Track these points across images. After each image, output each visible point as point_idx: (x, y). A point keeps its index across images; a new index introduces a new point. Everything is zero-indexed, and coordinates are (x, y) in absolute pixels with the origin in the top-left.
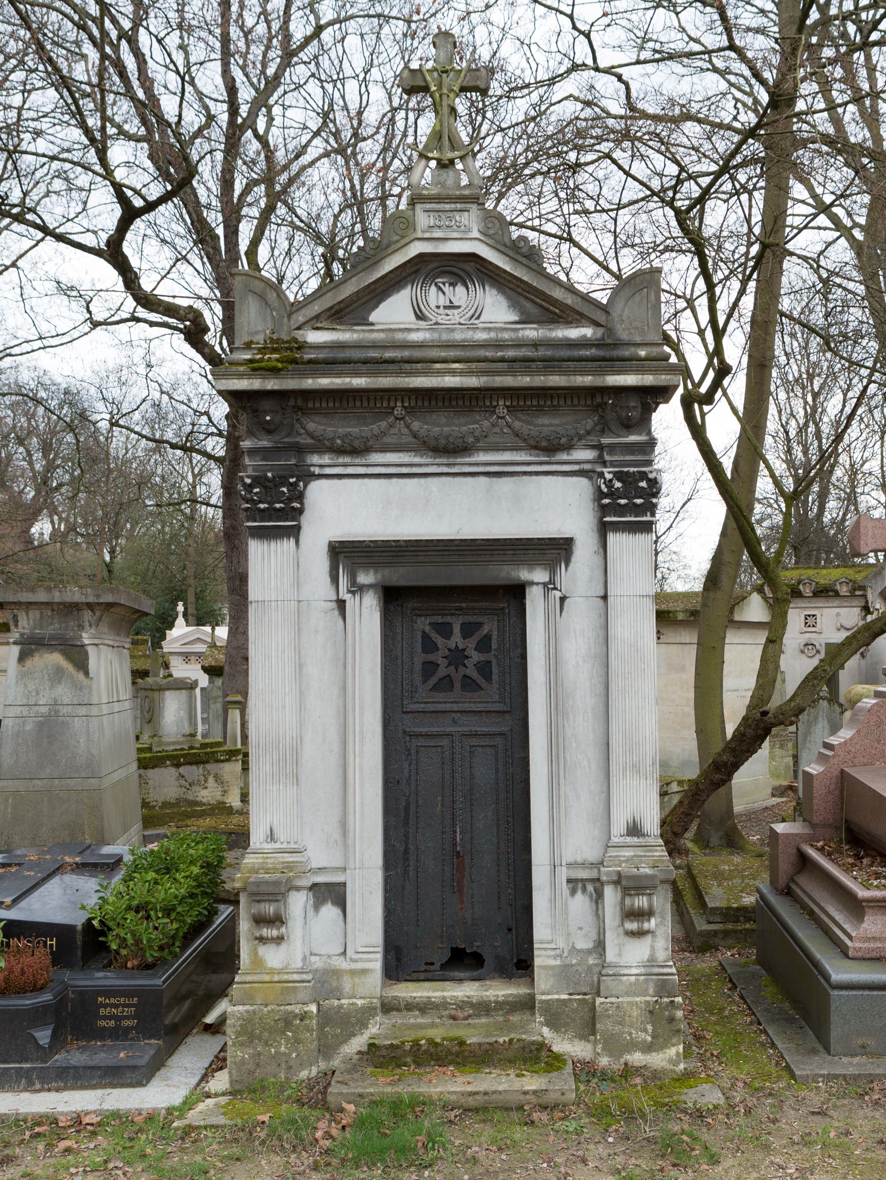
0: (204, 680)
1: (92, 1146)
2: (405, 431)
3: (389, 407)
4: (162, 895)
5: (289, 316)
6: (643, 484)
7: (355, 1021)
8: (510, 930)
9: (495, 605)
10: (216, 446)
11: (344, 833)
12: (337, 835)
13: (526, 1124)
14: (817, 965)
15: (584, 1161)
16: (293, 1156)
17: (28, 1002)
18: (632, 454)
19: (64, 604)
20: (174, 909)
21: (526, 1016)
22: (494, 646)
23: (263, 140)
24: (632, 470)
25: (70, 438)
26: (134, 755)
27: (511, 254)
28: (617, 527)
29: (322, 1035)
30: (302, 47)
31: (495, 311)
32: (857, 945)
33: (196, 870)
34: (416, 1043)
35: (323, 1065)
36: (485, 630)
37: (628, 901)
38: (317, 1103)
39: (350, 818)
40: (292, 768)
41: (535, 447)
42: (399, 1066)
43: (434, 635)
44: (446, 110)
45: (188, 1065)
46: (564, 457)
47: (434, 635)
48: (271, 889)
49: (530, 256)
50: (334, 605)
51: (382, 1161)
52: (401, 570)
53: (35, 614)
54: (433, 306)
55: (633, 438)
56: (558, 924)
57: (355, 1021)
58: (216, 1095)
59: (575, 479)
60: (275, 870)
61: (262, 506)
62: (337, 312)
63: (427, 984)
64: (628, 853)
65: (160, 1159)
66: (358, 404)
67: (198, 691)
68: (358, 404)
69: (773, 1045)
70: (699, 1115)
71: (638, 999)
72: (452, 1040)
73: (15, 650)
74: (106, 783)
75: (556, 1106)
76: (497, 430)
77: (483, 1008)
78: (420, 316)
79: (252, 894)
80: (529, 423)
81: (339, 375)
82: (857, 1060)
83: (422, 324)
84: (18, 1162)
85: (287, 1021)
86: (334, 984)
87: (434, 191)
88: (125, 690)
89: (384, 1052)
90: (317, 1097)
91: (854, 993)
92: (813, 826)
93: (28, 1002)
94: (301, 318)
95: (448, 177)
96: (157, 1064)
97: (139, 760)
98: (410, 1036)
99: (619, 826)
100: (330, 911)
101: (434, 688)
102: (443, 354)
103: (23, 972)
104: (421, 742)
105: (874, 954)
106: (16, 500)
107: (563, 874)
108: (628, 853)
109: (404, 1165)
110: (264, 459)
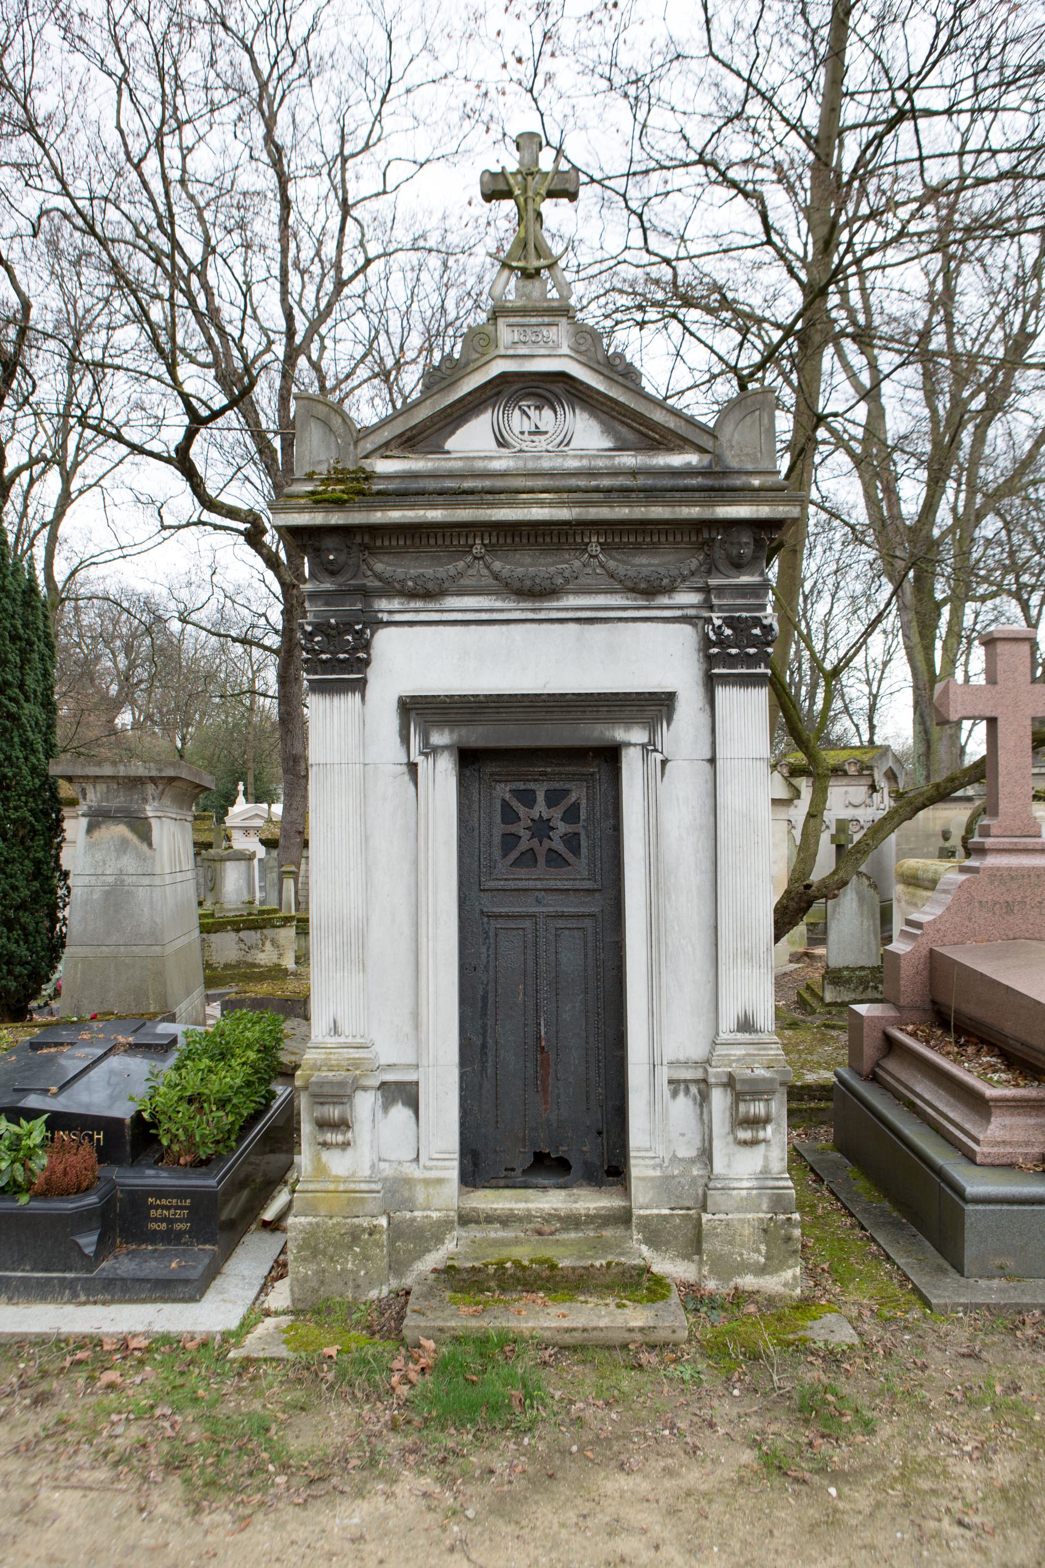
0: (261, 851)
1: (138, 1380)
2: (485, 572)
3: (466, 545)
4: (216, 1088)
5: (356, 443)
6: (757, 631)
7: (427, 1236)
8: (600, 1133)
9: (584, 770)
10: (273, 641)
11: (417, 1027)
12: (408, 1028)
13: (633, 1368)
14: (939, 1172)
15: (712, 1425)
16: (367, 1407)
17: (69, 1205)
18: (744, 597)
19: (128, 777)
20: (229, 1100)
21: (619, 1232)
22: (583, 815)
23: (316, 366)
24: (744, 614)
25: (148, 641)
26: (195, 922)
27: (606, 372)
28: (727, 680)
29: (393, 1250)
30: (352, 278)
31: (585, 437)
32: (986, 1150)
33: (252, 1055)
34: (500, 1265)
35: (394, 1283)
36: (573, 798)
37: (742, 1107)
38: (389, 1331)
39: (423, 1010)
40: (357, 952)
41: (633, 590)
42: (482, 1291)
43: (515, 804)
44: (531, 215)
45: (246, 1273)
46: (665, 600)
47: (515, 804)
48: (335, 1091)
49: (626, 374)
50: (404, 769)
51: (472, 1421)
52: (480, 729)
53: (101, 787)
54: (516, 431)
55: (745, 579)
56: (658, 1130)
57: (427, 1236)
58: (277, 1314)
59: (677, 626)
60: (338, 1067)
61: (324, 656)
62: (409, 439)
63: (507, 1192)
64: (740, 1051)
65: (212, 1406)
66: (432, 541)
67: (256, 862)
68: (432, 541)
69: (888, 1258)
70: (833, 1358)
71: (750, 1216)
72: (541, 1262)
73: (84, 822)
74: (169, 949)
75: (666, 1344)
76: (589, 570)
77: (572, 1221)
78: (502, 443)
79: (314, 1095)
80: (625, 563)
81: (412, 507)
82: (995, 1283)
83: (504, 451)
84: (55, 1401)
85: (354, 1236)
86: (406, 1194)
87: (519, 303)
88: (187, 861)
89: (465, 1276)
90: (389, 1321)
91: (991, 1207)
92: (898, 1007)
93: (69, 1205)
94: (368, 445)
95: (534, 288)
96: (213, 1272)
97: (202, 925)
98: (493, 1256)
99: (728, 1021)
100: (400, 1113)
101: (516, 863)
102: (530, 483)
103: (65, 1173)
104: (500, 924)
105: (1004, 1161)
106: (105, 696)
107: (664, 1074)
108: (740, 1051)
109: (499, 1427)
110: (327, 604)
